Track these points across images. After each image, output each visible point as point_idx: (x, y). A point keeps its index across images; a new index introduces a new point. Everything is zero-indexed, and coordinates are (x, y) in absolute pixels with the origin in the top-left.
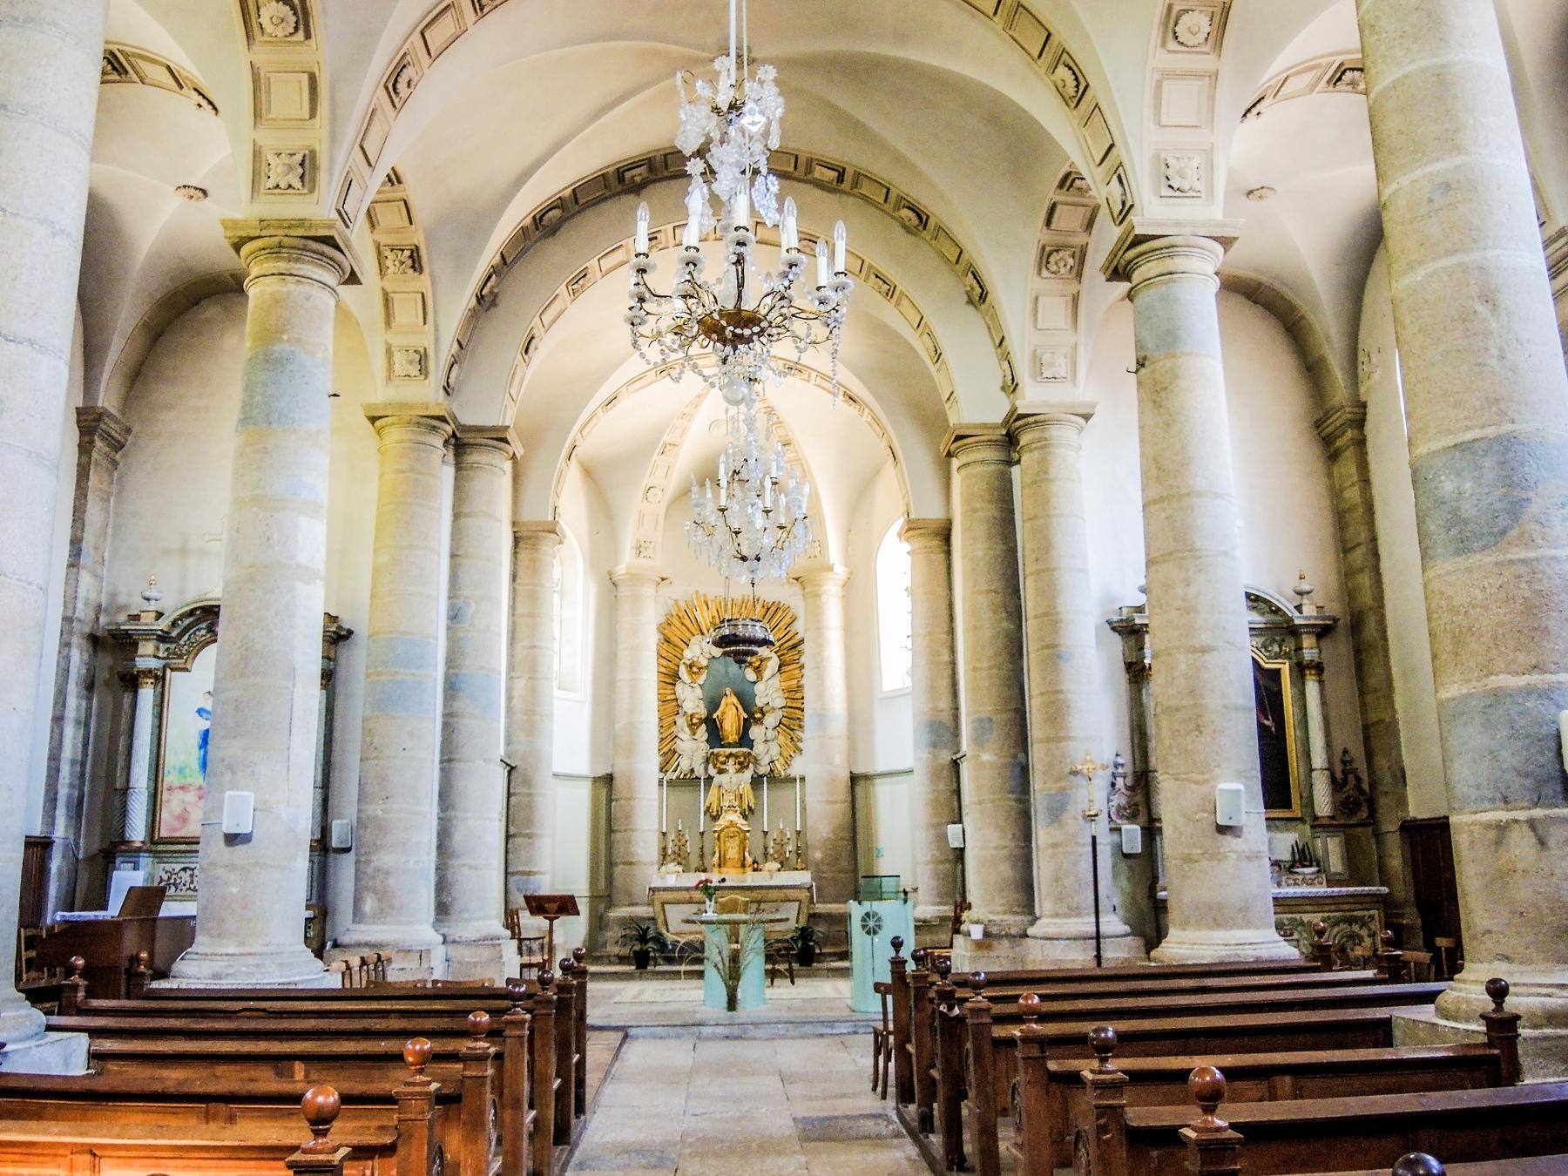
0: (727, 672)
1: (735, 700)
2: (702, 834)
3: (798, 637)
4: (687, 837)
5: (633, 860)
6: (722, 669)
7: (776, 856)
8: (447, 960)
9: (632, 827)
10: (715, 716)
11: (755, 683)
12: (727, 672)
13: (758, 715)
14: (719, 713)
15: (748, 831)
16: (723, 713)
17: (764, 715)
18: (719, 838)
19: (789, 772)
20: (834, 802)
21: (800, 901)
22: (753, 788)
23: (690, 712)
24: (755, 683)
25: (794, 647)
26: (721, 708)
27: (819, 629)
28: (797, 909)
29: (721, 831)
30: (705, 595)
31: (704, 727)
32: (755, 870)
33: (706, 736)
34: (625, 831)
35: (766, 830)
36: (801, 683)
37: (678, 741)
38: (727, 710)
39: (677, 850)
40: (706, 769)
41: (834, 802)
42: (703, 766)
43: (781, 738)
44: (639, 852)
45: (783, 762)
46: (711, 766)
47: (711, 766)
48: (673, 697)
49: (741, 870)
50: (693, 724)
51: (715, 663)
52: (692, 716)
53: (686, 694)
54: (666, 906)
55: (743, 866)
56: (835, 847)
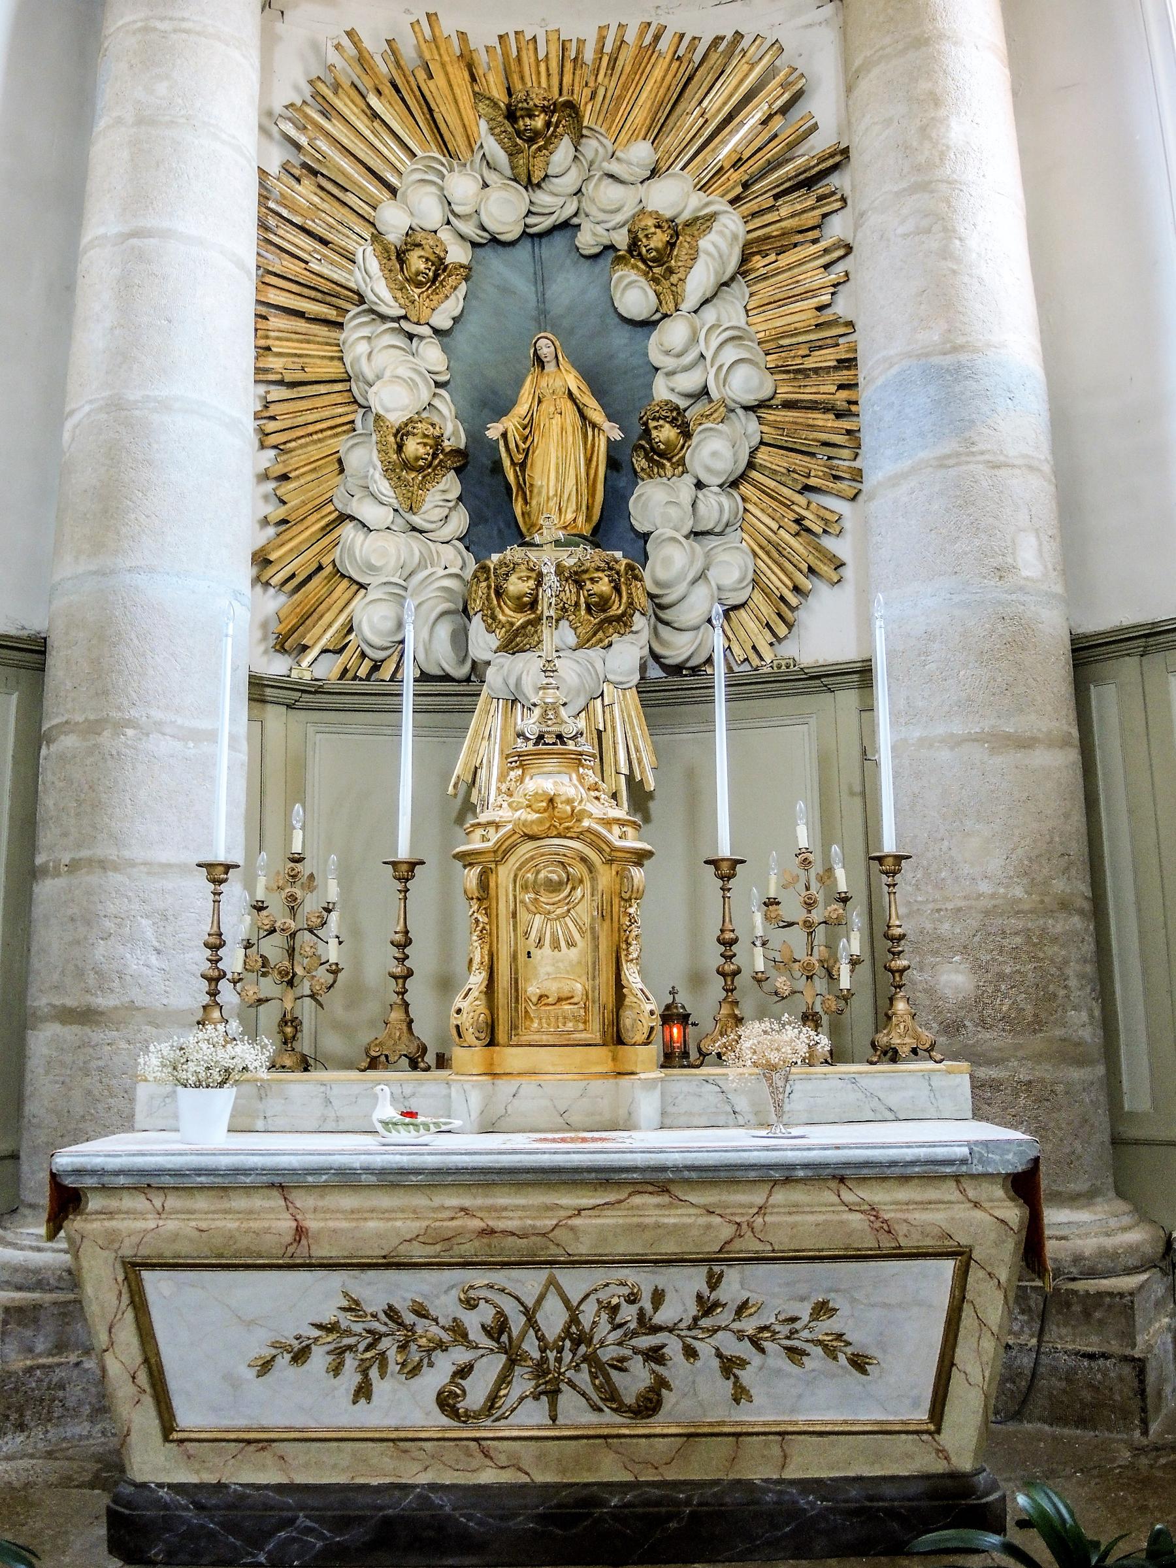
0: (542, 298)
1: (572, 381)
2: (406, 871)
3: (820, 143)
4: (332, 891)
5: (102, 1002)
6: (523, 286)
7: (781, 983)
8: (373, 1064)
9: (110, 852)
10: (493, 432)
11: (648, 325)
12: (542, 298)
13: (666, 433)
14: (511, 423)
15: (640, 857)
16: (529, 425)
17: (687, 434)
18: (484, 893)
19: (788, 650)
20: (1025, 743)
21: (963, 1257)
22: (653, 726)
23: (395, 418)
24: (648, 325)
25: (807, 182)
26: (522, 409)
27: (921, 42)
28: (943, 1300)
29: (502, 853)
30: (462, 35)
31: (450, 485)
32: (672, 1058)
33: (460, 521)
34: (74, 866)
35: (725, 850)
36: (841, 308)
37: (348, 531)
38: (541, 419)
39: (272, 948)
40: (460, 639)
41: (1025, 743)
42: (444, 631)
43: (761, 519)
44: (134, 966)
45: (767, 611)
46: (477, 625)
47: (477, 625)
48: (332, 370)
49: (600, 1058)
50: (407, 465)
51: (496, 264)
52: (402, 433)
53: (381, 359)
54: (155, 1284)
55: (616, 1038)
56: (1036, 941)
